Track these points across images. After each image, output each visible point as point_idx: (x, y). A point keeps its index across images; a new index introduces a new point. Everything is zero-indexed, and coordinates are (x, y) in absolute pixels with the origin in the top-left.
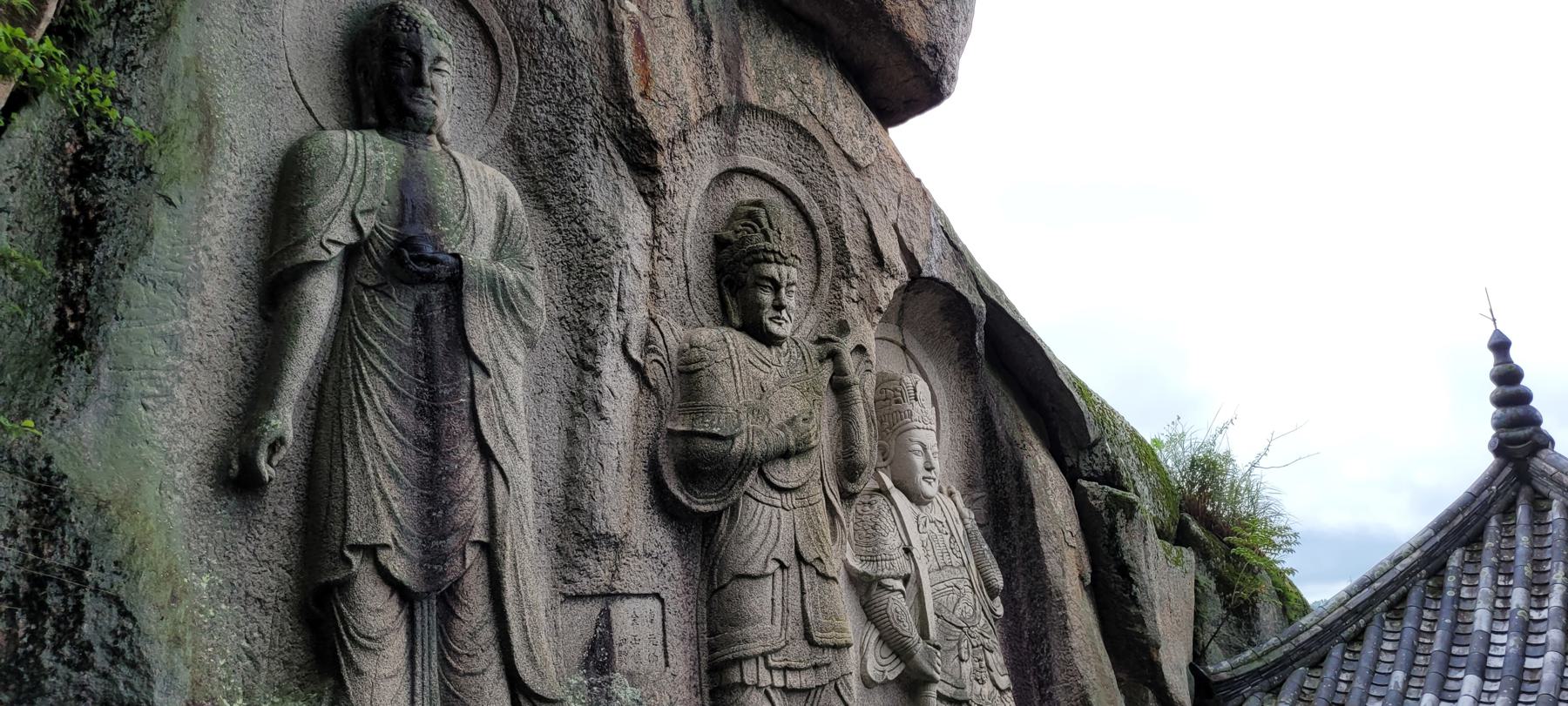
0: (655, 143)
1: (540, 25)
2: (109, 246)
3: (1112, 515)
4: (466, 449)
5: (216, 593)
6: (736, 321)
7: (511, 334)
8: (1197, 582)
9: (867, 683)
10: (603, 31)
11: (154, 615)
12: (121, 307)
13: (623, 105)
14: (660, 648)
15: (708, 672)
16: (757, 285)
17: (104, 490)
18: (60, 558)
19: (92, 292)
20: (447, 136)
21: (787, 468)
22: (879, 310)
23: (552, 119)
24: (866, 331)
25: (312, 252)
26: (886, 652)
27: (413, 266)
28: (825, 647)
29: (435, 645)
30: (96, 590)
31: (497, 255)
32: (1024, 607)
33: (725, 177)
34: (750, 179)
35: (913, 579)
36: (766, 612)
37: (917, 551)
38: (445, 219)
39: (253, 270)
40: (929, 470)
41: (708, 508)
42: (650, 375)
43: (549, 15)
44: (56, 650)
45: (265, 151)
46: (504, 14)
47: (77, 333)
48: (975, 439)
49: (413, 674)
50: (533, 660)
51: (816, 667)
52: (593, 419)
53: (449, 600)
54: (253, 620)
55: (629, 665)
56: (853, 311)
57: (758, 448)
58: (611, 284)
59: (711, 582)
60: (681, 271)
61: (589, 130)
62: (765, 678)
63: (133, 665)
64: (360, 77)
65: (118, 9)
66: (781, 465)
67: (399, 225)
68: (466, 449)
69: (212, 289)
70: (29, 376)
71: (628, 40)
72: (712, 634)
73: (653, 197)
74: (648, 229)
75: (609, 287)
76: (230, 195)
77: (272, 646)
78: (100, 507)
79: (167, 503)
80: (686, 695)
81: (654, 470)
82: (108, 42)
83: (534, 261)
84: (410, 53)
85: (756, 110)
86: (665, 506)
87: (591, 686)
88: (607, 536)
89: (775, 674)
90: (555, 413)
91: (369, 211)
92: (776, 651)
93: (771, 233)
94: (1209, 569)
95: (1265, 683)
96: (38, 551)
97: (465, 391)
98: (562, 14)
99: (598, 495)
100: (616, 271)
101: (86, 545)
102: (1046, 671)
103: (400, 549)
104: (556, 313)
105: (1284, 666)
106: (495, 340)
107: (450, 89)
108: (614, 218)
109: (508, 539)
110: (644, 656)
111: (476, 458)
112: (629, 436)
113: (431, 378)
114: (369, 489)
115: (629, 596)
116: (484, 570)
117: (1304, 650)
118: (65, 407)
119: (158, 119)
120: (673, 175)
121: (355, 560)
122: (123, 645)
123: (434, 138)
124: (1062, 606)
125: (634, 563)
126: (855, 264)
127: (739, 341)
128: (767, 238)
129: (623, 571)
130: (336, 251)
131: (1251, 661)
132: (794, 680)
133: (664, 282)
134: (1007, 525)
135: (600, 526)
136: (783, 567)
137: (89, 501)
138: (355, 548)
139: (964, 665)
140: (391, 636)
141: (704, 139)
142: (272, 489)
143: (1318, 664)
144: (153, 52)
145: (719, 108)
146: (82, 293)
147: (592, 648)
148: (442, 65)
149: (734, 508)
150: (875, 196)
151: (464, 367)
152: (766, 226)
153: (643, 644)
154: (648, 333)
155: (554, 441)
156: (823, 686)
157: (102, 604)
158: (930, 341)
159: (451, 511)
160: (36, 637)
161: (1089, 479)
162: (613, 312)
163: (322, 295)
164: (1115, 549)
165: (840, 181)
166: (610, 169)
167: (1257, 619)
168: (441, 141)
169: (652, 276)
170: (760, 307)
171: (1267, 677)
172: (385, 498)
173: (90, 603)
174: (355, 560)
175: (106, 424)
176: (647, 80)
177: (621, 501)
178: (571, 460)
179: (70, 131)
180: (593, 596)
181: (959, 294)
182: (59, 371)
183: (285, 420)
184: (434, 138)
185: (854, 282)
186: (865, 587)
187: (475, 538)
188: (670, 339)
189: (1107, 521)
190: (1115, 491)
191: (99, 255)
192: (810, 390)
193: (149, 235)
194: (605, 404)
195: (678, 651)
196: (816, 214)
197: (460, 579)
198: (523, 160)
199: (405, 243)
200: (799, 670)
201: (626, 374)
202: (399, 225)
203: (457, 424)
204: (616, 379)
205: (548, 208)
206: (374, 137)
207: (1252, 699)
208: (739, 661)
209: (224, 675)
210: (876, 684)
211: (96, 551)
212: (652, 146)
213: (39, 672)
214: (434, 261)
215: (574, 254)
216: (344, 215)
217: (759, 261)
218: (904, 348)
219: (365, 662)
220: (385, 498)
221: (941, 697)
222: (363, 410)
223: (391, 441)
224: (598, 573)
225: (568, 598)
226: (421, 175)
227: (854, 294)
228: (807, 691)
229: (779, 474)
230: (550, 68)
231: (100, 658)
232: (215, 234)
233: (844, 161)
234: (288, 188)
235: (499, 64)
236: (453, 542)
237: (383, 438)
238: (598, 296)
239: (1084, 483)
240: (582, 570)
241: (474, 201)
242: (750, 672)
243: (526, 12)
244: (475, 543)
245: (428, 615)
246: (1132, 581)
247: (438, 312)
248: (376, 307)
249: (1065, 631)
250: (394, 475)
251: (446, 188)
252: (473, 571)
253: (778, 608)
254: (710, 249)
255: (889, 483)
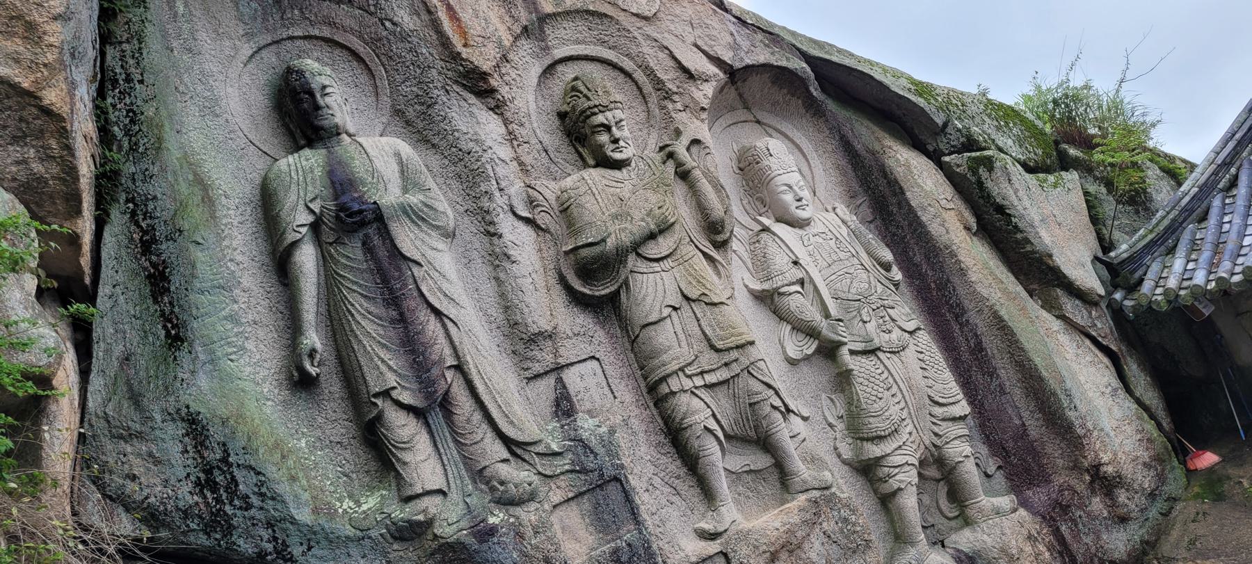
0: (485, 73)
1: (384, 33)
2: (176, 282)
3: (974, 171)
4: (423, 315)
5: (312, 448)
6: (591, 162)
7: (429, 235)
8: (1086, 193)
9: (792, 362)
10: (425, 17)
11: (274, 469)
12: (194, 312)
13: (454, 58)
14: (606, 389)
15: (648, 393)
16: (593, 133)
17: (223, 411)
18: (215, 455)
19: (176, 310)
20: (352, 131)
21: (657, 244)
22: (703, 109)
23: (415, 89)
24: (696, 127)
25: (291, 237)
26: (801, 336)
27: (349, 220)
28: (729, 349)
29: (447, 434)
30: (239, 466)
31: (405, 190)
32: (924, 267)
33: (549, 70)
34: (570, 64)
35: (807, 280)
36: (674, 343)
37: (804, 259)
38: (364, 185)
39: (267, 260)
40: (799, 200)
41: (607, 291)
42: (539, 222)
43: (387, 24)
44: (231, 504)
45: (248, 189)
46: (361, 37)
47: (177, 335)
48: (843, 163)
49: (440, 455)
50: (512, 423)
51: (726, 364)
52: (507, 265)
53: (446, 404)
54: (339, 455)
55: (588, 406)
56: (681, 118)
57: (626, 239)
58: (488, 176)
59: (629, 336)
60: (539, 146)
61: (439, 85)
62: (688, 384)
63: (273, 499)
64: (287, 120)
65: (131, 149)
66: (651, 244)
67: (336, 199)
68: (423, 315)
69: (247, 281)
70: (162, 367)
71: (442, 15)
72: (642, 369)
73: (498, 108)
74: (503, 130)
75: (488, 179)
76: (235, 223)
77: (356, 465)
78: (224, 423)
79: (264, 408)
80: (637, 411)
81: (562, 280)
82: (133, 169)
83: (430, 183)
84: (306, 93)
85: (554, 16)
86: (578, 300)
87: (562, 427)
88: (540, 333)
89: (695, 379)
90: (482, 270)
91: (314, 199)
92: (689, 364)
93: (589, 95)
94: (1096, 178)
95: (1163, 248)
96: (202, 457)
97: (411, 280)
98: (395, 19)
99: (526, 310)
100: (488, 166)
101: (224, 445)
102: (958, 305)
103: (403, 387)
104: (462, 209)
105: (1174, 229)
106: (418, 243)
107: (341, 99)
108: (476, 133)
109: (468, 358)
110: (597, 398)
111: (432, 318)
112: (538, 265)
113: (385, 281)
114: (372, 359)
115: (572, 364)
116: (461, 381)
117: (1188, 211)
118: (185, 376)
119: (175, 200)
120: (507, 88)
121: (379, 402)
122: (264, 490)
123: (344, 136)
124: (953, 255)
125: (568, 343)
126: (670, 85)
127: (595, 176)
128: (589, 99)
129: (562, 351)
130: (304, 230)
131: (1145, 236)
132: (711, 378)
133: (527, 159)
134: (890, 214)
135: (534, 329)
136: (675, 309)
137: (217, 421)
138: (376, 395)
139: (868, 325)
140: (418, 437)
141: (522, 53)
142: (322, 379)
143: (1204, 218)
144: (158, 164)
145: (525, 28)
146: (172, 312)
147: (557, 403)
148: (328, 90)
149: (626, 282)
150: (670, 32)
151: (404, 267)
152: (585, 91)
153: (593, 391)
154: (529, 196)
155: (488, 288)
156: (738, 375)
157: (244, 472)
158: (775, 108)
159: (427, 354)
160: (218, 500)
161: (949, 154)
162: (497, 194)
163: (307, 258)
164: (988, 197)
165: (636, 34)
166: (463, 103)
167: (1151, 200)
168: (350, 135)
169: (517, 159)
170: (601, 146)
171: (1162, 244)
172: (383, 361)
173: (239, 475)
174: (379, 402)
175: (213, 377)
176: (464, 34)
177: (543, 305)
178: (502, 295)
179: (133, 227)
180: (546, 373)
181: (778, 67)
182: (175, 358)
183: (313, 338)
184: (344, 136)
185: (676, 98)
186: (768, 299)
187: (449, 364)
188: (548, 194)
189: (973, 179)
190: (973, 154)
191: (173, 288)
192: (659, 185)
193: (194, 267)
194: (511, 252)
195: (622, 387)
196: (628, 65)
197: (447, 392)
198: (408, 123)
199: (342, 208)
200: (714, 370)
201: (526, 232)
202: (336, 199)
203: (412, 303)
204: (519, 240)
205: (434, 146)
206: (307, 152)
207: (1154, 265)
208: (664, 379)
209: (332, 489)
210: (799, 361)
211: (230, 446)
212: (484, 76)
213: (228, 518)
214: (360, 212)
215: (460, 167)
216: (301, 207)
217: (589, 117)
218: (758, 122)
219: (407, 457)
220: (383, 361)
221: (852, 352)
222: (352, 315)
223: (375, 327)
224: (544, 358)
225: (529, 379)
226: (340, 163)
227: (679, 106)
228: (726, 382)
229: (652, 250)
230: (400, 57)
231: (255, 500)
232: (235, 249)
233: (634, 19)
234: (267, 203)
235: (370, 70)
236: (435, 372)
237: (370, 327)
238: (483, 188)
239: (947, 159)
240: (532, 359)
241: (379, 164)
242: (674, 384)
243: (373, 29)
244: (449, 367)
245: (437, 418)
246: (1010, 215)
247: (376, 241)
248: (339, 253)
249: (963, 272)
250: (383, 346)
251: (358, 167)
252: (454, 384)
253: (682, 337)
254: (557, 123)
255: (766, 221)
